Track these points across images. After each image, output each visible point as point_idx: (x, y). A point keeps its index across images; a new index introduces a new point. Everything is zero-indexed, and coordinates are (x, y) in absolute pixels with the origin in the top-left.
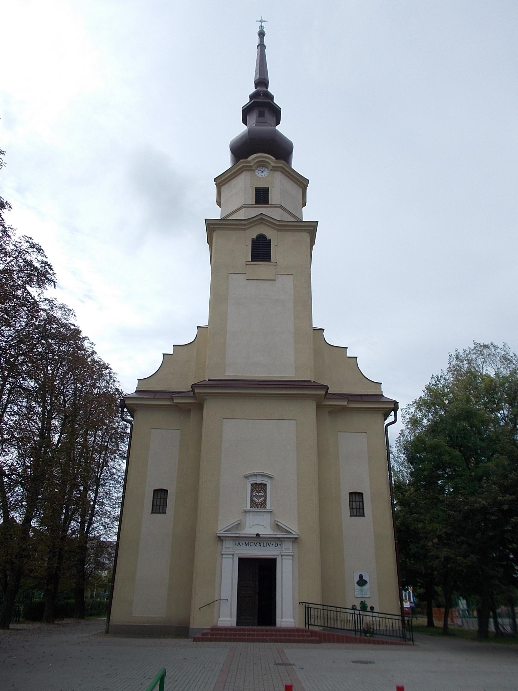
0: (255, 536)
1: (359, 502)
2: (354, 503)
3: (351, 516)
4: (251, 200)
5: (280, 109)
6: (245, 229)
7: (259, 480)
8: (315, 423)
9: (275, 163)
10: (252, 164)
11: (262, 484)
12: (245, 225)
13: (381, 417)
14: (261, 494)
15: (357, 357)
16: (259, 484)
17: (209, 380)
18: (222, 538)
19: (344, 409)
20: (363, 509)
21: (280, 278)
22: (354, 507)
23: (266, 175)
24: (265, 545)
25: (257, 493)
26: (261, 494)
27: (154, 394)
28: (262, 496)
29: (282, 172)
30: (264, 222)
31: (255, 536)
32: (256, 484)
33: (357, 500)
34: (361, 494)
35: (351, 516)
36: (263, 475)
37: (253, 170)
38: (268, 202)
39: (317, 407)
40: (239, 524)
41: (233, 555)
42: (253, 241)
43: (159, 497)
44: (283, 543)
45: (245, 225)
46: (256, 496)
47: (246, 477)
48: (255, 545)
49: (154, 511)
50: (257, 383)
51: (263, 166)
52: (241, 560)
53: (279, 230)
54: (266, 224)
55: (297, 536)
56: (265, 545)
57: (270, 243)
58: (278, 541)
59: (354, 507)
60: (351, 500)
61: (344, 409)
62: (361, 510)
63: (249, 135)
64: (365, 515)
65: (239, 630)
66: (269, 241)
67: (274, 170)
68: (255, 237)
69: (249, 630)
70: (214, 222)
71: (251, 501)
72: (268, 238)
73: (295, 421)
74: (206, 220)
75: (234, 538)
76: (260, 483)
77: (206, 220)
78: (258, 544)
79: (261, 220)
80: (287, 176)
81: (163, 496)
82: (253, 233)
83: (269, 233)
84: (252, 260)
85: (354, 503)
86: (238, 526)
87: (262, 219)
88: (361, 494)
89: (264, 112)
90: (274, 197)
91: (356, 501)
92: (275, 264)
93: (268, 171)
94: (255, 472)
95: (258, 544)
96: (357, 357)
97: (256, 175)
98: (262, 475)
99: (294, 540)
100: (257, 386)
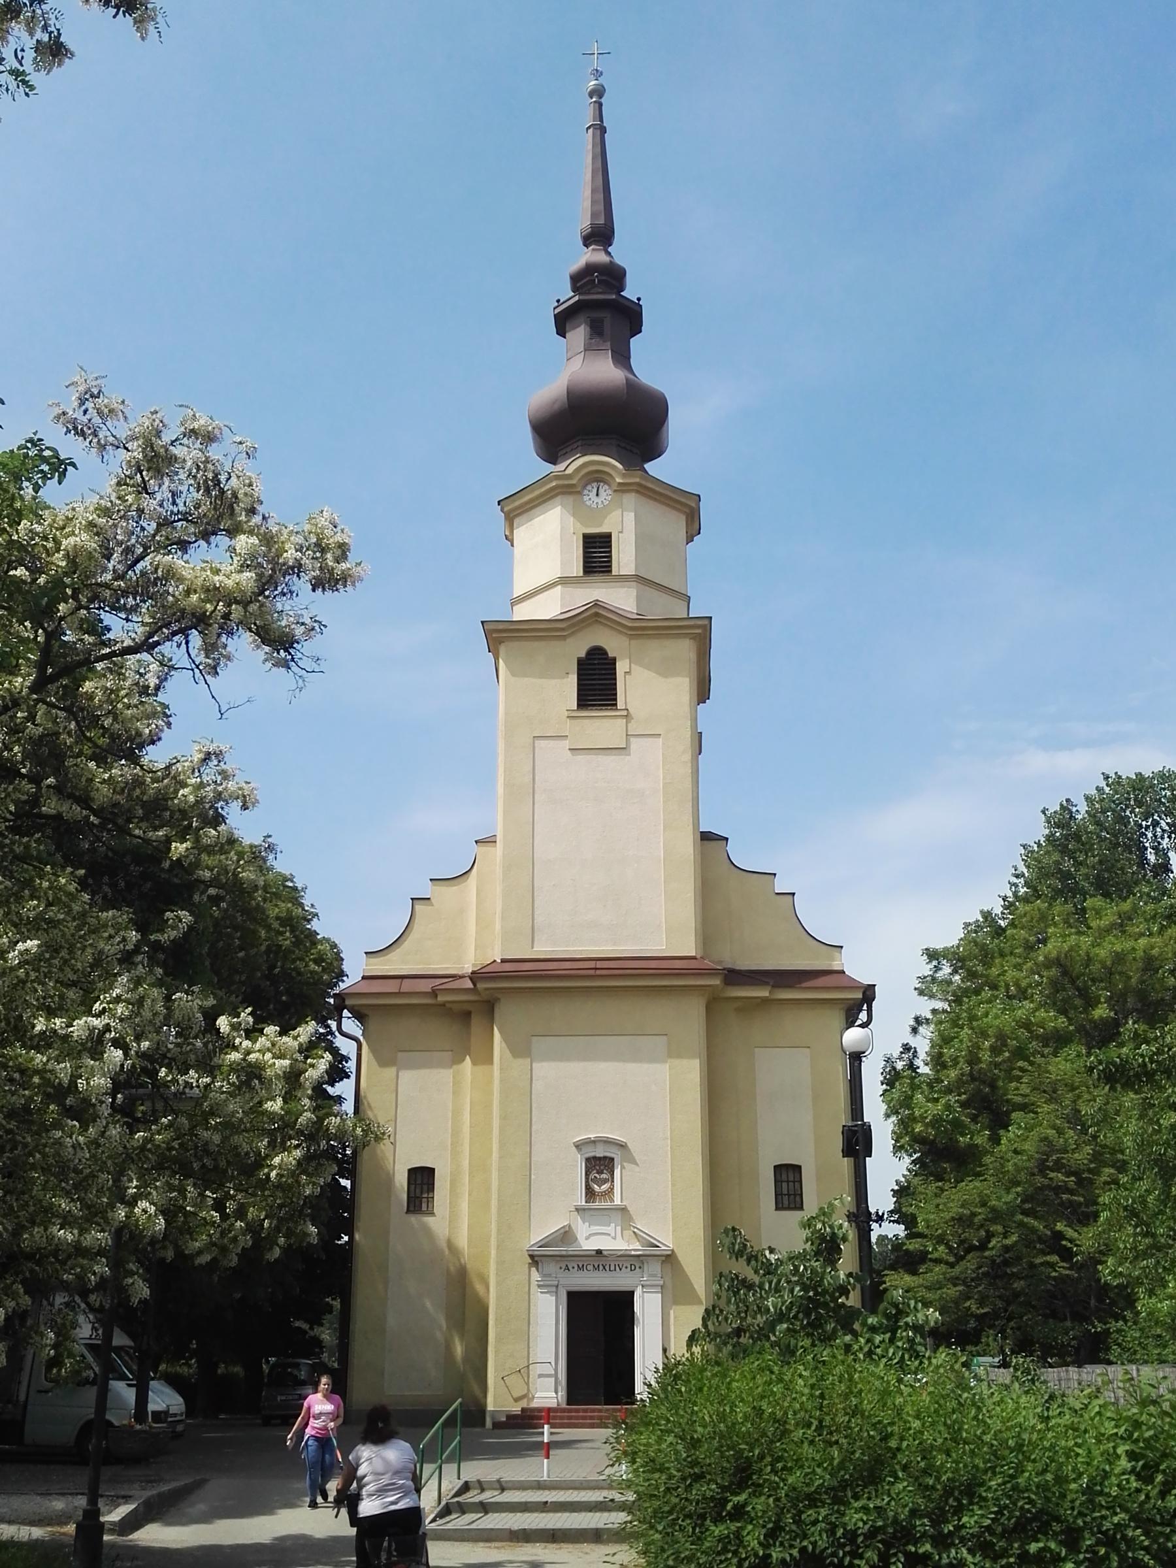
0: (594, 1253)
1: (794, 1182)
2: (784, 1185)
3: (777, 1209)
4: (576, 567)
5: (637, 308)
6: (564, 638)
7: (600, 1152)
8: (703, 1033)
9: (624, 476)
10: (574, 482)
11: (605, 1158)
12: (563, 629)
13: (836, 1018)
14: (604, 1176)
15: (793, 894)
16: (600, 1159)
17: (503, 961)
18: (536, 1259)
19: (764, 1003)
20: (801, 1195)
21: (635, 743)
22: (785, 1192)
23: (606, 503)
24: (612, 1268)
25: (597, 1175)
26: (604, 1176)
27: (400, 980)
28: (605, 1181)
29: (637, 492)
30: (602, 620)
31: (594, 1253)
32: (595, 1158)
33: (791, 1178)
34: (797, 1169)
35: (777, 1209)
36: (608, 1142)
37: (579, 493)
38: (610, 571)
39: (709, 1008)
40: (566, 1232)
41: (557, 1286)
42: (580, 662)
43: (419, 1182)
44: (645, 1265)
45: (563, 629)
46: (595, 1180)
47: (578, 1146)
48: (596, 1268)
49: (412, 1209)
50: (592, 964)
51: (598, 481)
52: (572, 1296)
53: (631, 637)
54: (606, 625)
55: (669, 1253)
56: (612, 1268)
57: (615, 664)
58: (635, 1261)
59: (785, 1192)
60: (778, 1178)
61: (764, 1003)
62: (798, 1198)
63: (568, 393)
64: (805, 1207)
65: (570, 1411)
66: (613, 662)
67: (624, 491)
68: (583, 654)
69: (585, 1411)
70: (501, 627)
71: (586, 1188)
72: (611, 655)
73: (665, 1037)
74: (483, 622)
75: (559, 1258)
76: (602, 1155)
77: (483, 622)
78: (601, 1267)
79: (596, 615)
80: (650, 497)
81: (425, 1181)
82: (579, 647)
83: (612, 644)
84: (579, 705)
85: (784, 1185)
86: (566, 1235)
87: (597, 614)
88: (797, 1169)
89: (602, 321)
90: (624, 558)
91: (788, 1182)
92: (625, 713)
93: (610, 492)
94: (592, 1136)
95: (601, 1267)
96: (793, 894)
97: (584, 502)
98: (605, 1142)
99: (664, 1258)
100: (592, 972)
